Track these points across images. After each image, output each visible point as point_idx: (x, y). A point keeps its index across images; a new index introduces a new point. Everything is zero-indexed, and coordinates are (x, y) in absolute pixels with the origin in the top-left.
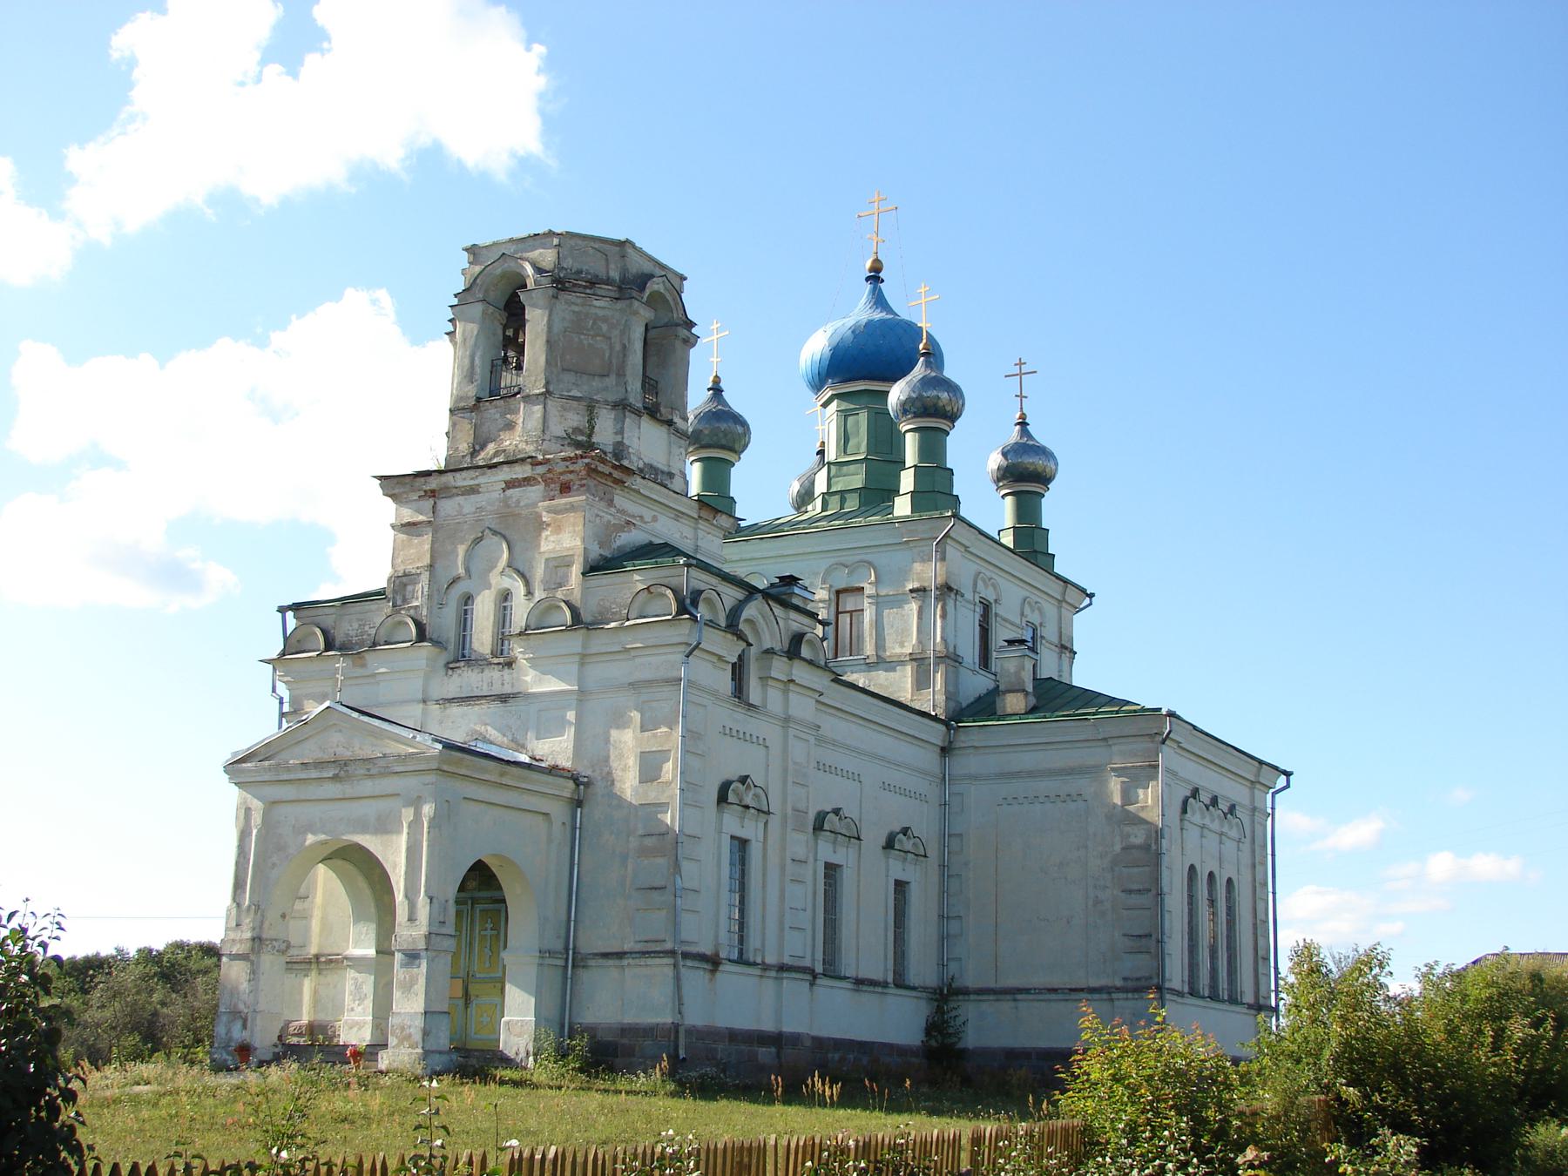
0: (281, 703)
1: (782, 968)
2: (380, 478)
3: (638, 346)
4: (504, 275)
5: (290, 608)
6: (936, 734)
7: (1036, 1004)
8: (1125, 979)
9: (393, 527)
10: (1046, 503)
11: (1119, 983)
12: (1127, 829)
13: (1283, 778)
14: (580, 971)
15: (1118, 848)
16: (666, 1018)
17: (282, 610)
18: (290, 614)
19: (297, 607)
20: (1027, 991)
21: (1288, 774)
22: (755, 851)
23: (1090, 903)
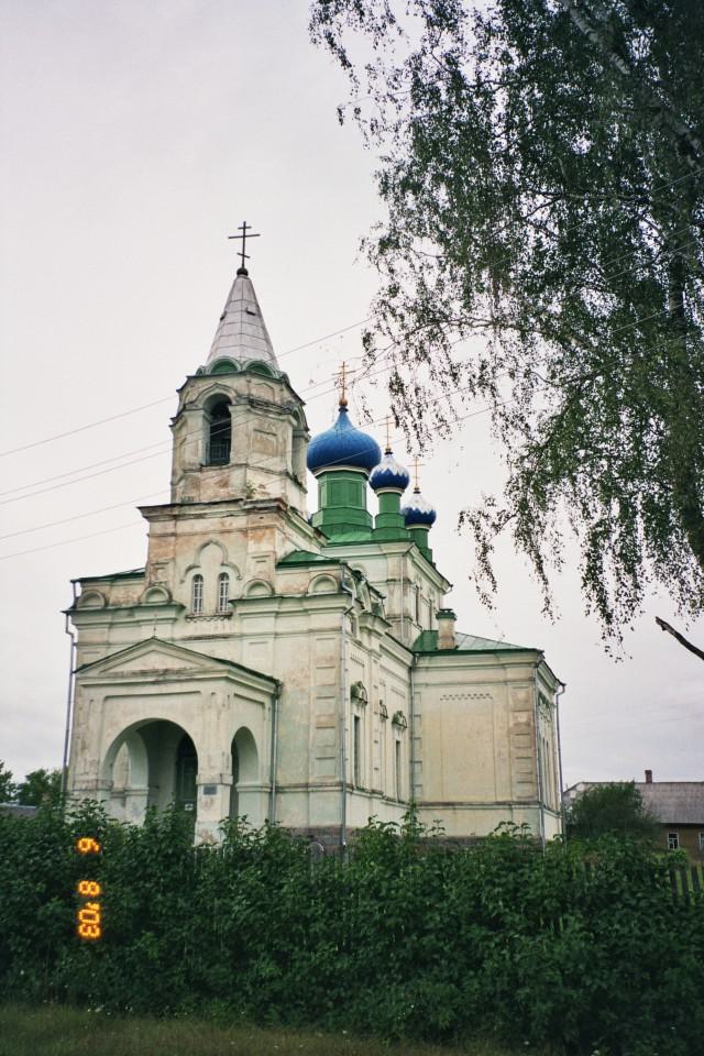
0: (73, 637)
1: (373, 792)
2: (140, 508)
3: (290, 440)
4: (216, 396)
5: (78, 581)
6: (408, 659)
7: (467, 812)
8: (519, 797)
9: (148, 535)
10: (429, 534)
11: (515, 799)
12: (516, 714)
13: (561, 687)
14: (279, 795)
15: (511, 724)
16: (336, 822)
17: (74, 582)
18: (78, 584)
19: (83, 581)
20: (461, 804)
21: (563, 685)
22: (361, 721)
23: (496, 754)
